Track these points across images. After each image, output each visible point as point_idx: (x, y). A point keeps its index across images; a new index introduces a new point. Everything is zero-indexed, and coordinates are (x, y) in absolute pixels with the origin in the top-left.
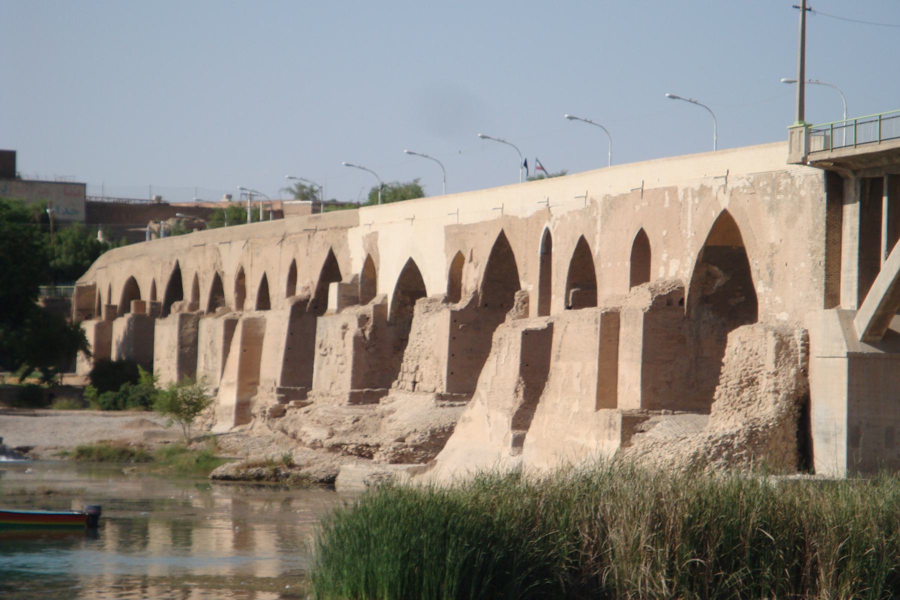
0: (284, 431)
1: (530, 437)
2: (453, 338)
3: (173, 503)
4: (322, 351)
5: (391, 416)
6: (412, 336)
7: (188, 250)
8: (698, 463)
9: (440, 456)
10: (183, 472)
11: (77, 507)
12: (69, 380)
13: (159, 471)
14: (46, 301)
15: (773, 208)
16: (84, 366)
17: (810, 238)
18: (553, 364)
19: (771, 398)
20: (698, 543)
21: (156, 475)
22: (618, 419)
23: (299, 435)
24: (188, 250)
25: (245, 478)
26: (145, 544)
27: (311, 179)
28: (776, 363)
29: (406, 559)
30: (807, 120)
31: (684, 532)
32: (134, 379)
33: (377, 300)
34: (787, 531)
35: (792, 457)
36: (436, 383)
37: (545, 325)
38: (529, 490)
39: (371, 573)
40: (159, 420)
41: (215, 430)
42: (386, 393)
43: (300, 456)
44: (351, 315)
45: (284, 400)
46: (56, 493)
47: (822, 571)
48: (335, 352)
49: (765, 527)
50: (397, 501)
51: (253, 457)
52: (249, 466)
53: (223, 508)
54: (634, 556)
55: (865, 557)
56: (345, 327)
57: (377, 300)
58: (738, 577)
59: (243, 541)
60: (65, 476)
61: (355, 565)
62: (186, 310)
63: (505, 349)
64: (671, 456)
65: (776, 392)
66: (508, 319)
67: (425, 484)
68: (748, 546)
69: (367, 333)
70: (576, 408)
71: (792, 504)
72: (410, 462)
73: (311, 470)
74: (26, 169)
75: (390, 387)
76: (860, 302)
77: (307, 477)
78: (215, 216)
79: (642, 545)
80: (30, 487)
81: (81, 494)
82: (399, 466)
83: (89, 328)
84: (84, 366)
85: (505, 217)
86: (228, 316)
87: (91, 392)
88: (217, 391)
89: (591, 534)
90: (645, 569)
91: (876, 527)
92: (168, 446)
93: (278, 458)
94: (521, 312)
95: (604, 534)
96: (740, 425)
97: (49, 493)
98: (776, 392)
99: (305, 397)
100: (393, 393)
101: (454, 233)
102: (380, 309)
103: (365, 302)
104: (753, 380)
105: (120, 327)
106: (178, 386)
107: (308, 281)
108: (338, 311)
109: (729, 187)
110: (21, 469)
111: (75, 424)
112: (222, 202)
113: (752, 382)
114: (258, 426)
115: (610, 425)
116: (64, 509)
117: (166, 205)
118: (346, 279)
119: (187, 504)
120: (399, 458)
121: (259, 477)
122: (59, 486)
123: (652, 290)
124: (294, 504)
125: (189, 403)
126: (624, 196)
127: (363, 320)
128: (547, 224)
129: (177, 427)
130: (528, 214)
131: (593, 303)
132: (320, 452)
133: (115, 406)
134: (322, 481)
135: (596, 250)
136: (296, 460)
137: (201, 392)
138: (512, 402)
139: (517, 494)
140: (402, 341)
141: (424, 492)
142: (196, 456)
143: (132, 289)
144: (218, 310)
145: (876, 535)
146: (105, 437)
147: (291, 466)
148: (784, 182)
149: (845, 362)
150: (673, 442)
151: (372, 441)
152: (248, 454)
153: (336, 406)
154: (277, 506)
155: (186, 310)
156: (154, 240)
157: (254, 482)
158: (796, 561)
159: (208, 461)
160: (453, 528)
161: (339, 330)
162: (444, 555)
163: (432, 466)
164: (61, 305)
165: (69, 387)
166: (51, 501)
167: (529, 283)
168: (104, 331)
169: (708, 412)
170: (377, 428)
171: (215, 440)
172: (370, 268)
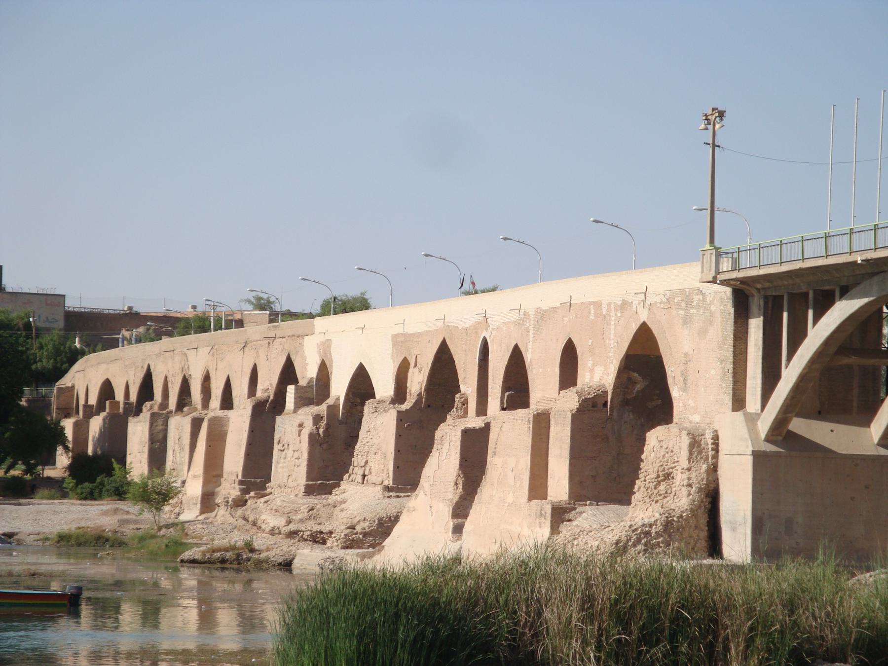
0: (245, 519)
1: (468, 526)
8: (621, 548)
10: (153, 556)
12: (49, 472)
16: (63, 460)
19: (685, 491)
20: (623, 621)
22: (548, 509)
23: (259, 523)
25: (210, 562)
32: (109, 471)
33: (330, 401)
35: (703, 544)
40: (131, 509)
44: (307, 415)
51: (217, 543)
56: (301, 425)
57: (330, 401)
59: (207, 620)
60: (46, 559)
62: (156, 409)
65: (690, 485)
66: (449, 418)
73: (270, 554)
76: (763, 407)
78: (182, 324)
80: (16, 569)
83: (68, 425)
84: (63, 460)
86: (195, 414)
87: (70, 483)
90: (576, 644)
92: (140, 533)
95: (540, 614)
100: (344, 485)
101: (401, 340)
102: (332, 409)
103: (319, 403)
105: (96, 425)
112: (187, 311)
113: (668, 476)
114: (222, 514)
117: (137, 314)
118: (302, 382)
119: (156, 585)
120: (350, 544)
121: (223, 561)
123: (579, 394)
127: (317, 419)
129: (148, 515)
131: (525, 404)
132: (278, 538)
133: (91, 496)
135: (528, 357)
136: (256, 545)
140: (353, 438)
143: (107, 390)
146: (83, 524)
147: (252, 550)
148: (696, 298)
149: (750, 459)
150: (597, 530)
151: (325, 528)
154: (238, 587)
155: (156, 409)
165: (49, 478)
167: (468, 386)
168: (81, 429)
169: (629, 503)
170: (330, 517)
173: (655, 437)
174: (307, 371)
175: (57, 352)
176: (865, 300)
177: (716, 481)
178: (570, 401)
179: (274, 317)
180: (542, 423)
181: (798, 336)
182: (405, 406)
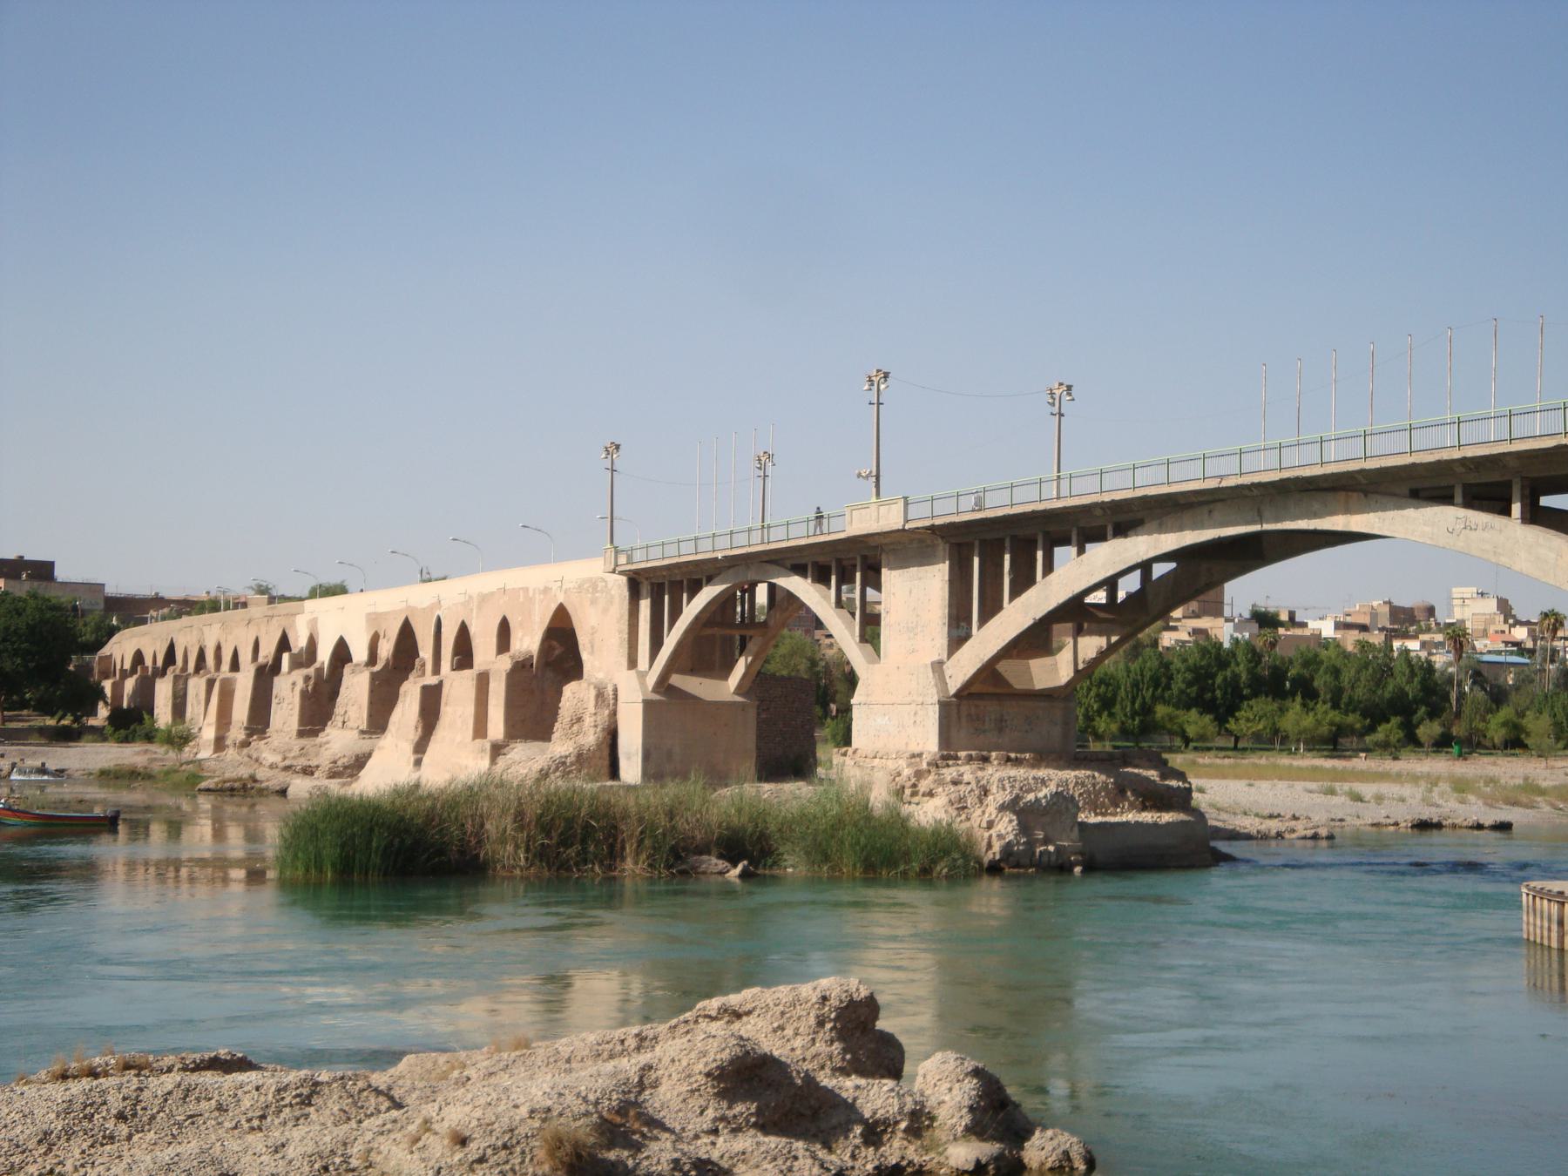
0: (250, 757)
1: (426, 759)
2: (372, 691)
3: (168, 807)
4: (277, 701)
5: (327, 746)
6: (342, 690)
7: (180, 630)
8: (544, 775)
9: (362, 773)
10: (176, 787)
11: (98, 811)
12: (92, 722)
13: (159, 785)
14: (75, 666)
15: (594, 602)
16: (103, 712)
17: (618, 622)
18: (443, 708)
19: (592, 730)
20: (546, 829)
21: (157, 788)
22: (488, 746)
23: (261, 759)
24: (180, 630)
26: (147, 835)
27: (268, 579)
28: (596, 706)
29: (343, 846)
30: (616, 543)
31: (537, 823)
32: (141, 721)
33: (317, 665)
34: (605, 820)
35: (605, 770)
36: (359, 722)
37: (437, 682)
38: (430, 795)
39: (318, 856)
40: (158, 750)
41: (199, 756)
42: (323, 730)
43: (262, 774)
44: (298, 676)
45: (250, 735)
46: (86, 801)
47: (628, 846)
48: (286, 702)
49: (591, 818)
50: (337, 805)
51: (227, 775)
52: (225, 782)
53: (206, 812)
54: (503, 840)
55: (656, 836)
56: (294, 684)
57: (317, 665)
58: (572, 852)
59: (219, 834)
60: (90, 789)
61: (307, 849)
62: (178, 672)
63: (408, 699)
64: (525, 771)
65: (596, 726)
67: (357, 793)
68: (579, 831)
69: (310, 688)
70: (458, 738)
71: (609, 802)
72: (340, 778)
73: (270, 784)
74: (61, 574)
75: (326, 725)
76: (650, 667)
77: (267, 789)
78: (198, 606)
79: (508, 832)
80: (67, 797)
81: (104, 802)
82: (332, 781)
83: (107, 685)
84: (103, 712)
85: (409, 607)
87: (109, 730)
88: (200, 729)
89: (473, 826)
90: (510, 848)
91: (663, 816)
92: (165, 768)
93: (246, 776)
94: (420, 673)
95: (482, 825)
96: (571, 750)
97: (81, 801)
98: (596, 726)
99: (265, 733)
100: (328, 729)
101: (373, 618)
102: (319, 671)
104: (580, 718)
105: (130, 685)
106: (172, 726)
107: (267, 651)
108: (289, 672)
109: (564, 587)
110: (60, 784)
111: (97, 753)
112: (203, 596)
113: (579, 719)
114: (231, 754)
115: (482, 751)
116: (88, 812)
117: (162, 598)
118: (295, 650)
119: (178, 808)
120: (333, 775)
121: (232, 789)
122: (88, 797)
123: (512, 657)
124: (257, 808)
125: (181, 738)
126: (492, 594)
127: (307, 679)
128: (438, 612)
129: (172, 755)
130: (425, 606)
133: (126, 740)
134: (277, 792)
135: (473, 630)
136: (258, 777)
137: (189, 730)
138: (413, 735)
139: (421, 798)
140: (335, 694)
141: (356, 798)
142: (186, 774)
143: (138, 658)
144: (201, 672)
145: (663, 821)
147: (255, 781)
148: (601, 585)
149: (640, 706)
150: (526, 761)
151: (313, 763)
152: (223, 773)
153: (287, 739)
154: (244, 810)
155: (178, 672)
156: (154, 624)
157: (228, 793)
158: (611, 840)
159: (194, 778)
160: (377, 824)
161: (289, 686)
162: (370, 841)
163: (356, 780)
164: (87, 669)
165: (92, 727)
166: (80, 807)
167: (426, 652)
168: (118, 688)
170: (317, 755)
171: (200, 765)
172: (312, 644)
173: (570, 691)
174: (299, 642)
175: (98, 628)
176: (724, 587)
177: (616, 723)
178: (505, 663)
179: (272, 600)
180: (483, 680)
181: (676, 613)
182: (378, 668)
